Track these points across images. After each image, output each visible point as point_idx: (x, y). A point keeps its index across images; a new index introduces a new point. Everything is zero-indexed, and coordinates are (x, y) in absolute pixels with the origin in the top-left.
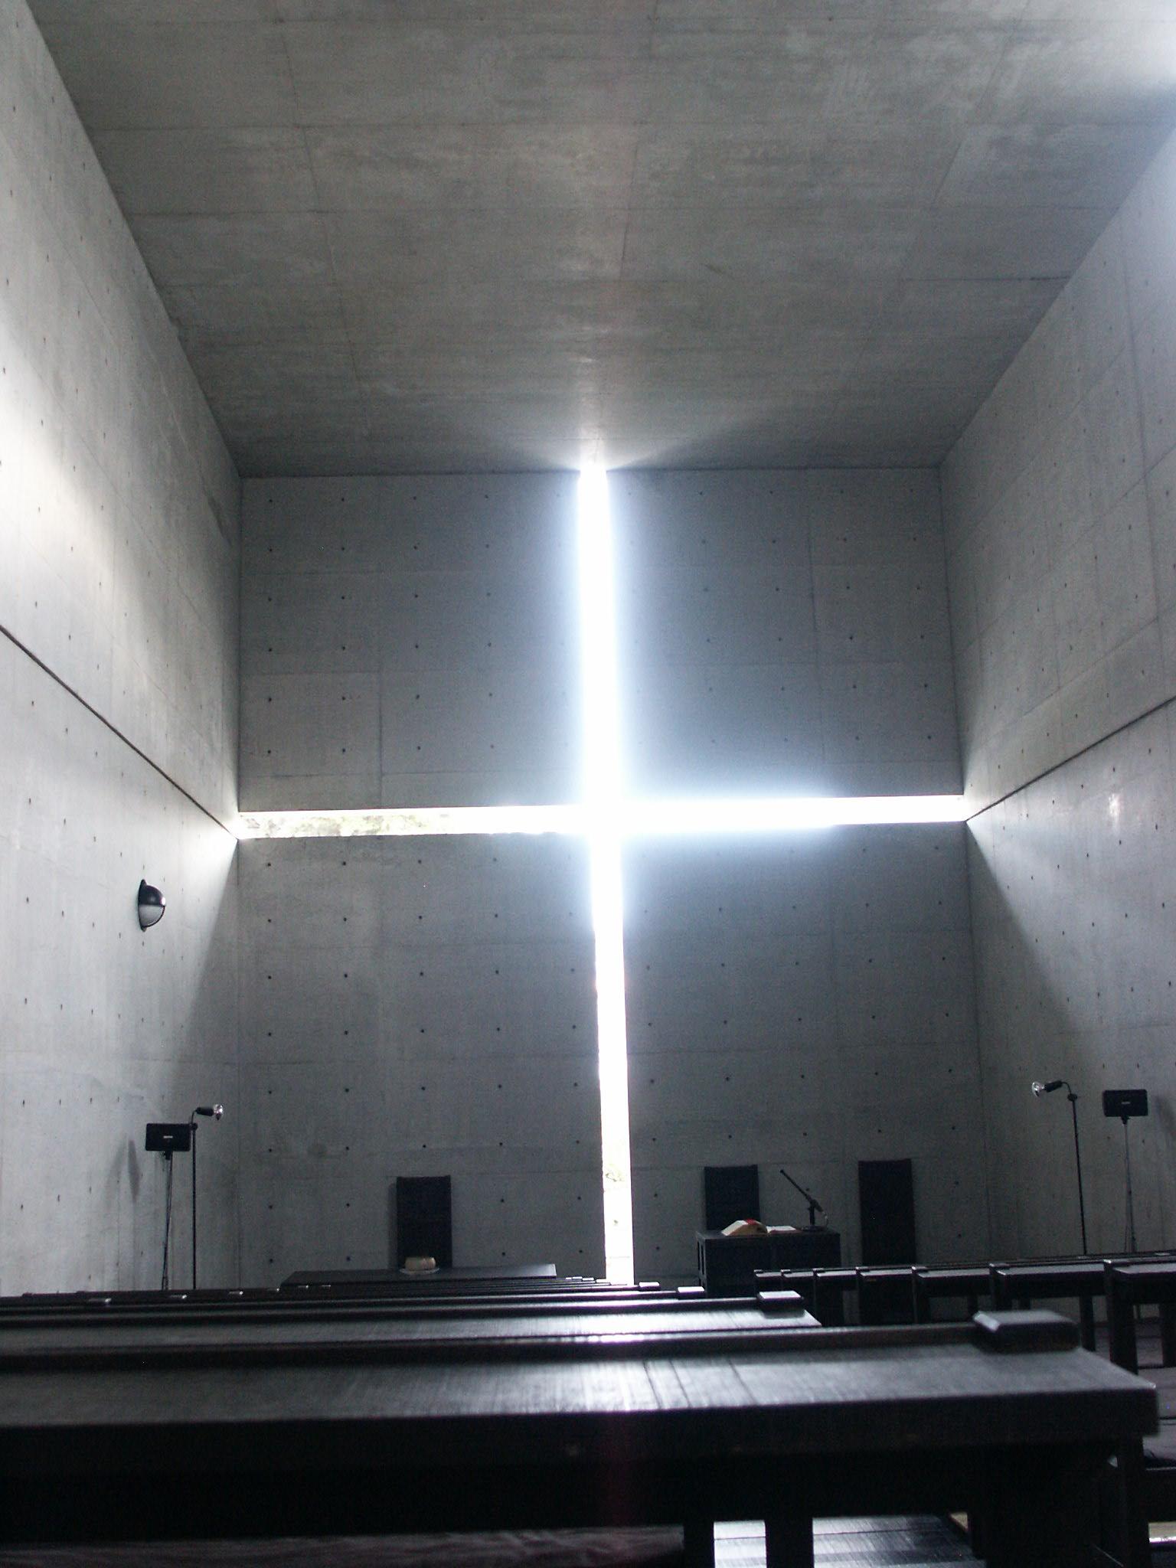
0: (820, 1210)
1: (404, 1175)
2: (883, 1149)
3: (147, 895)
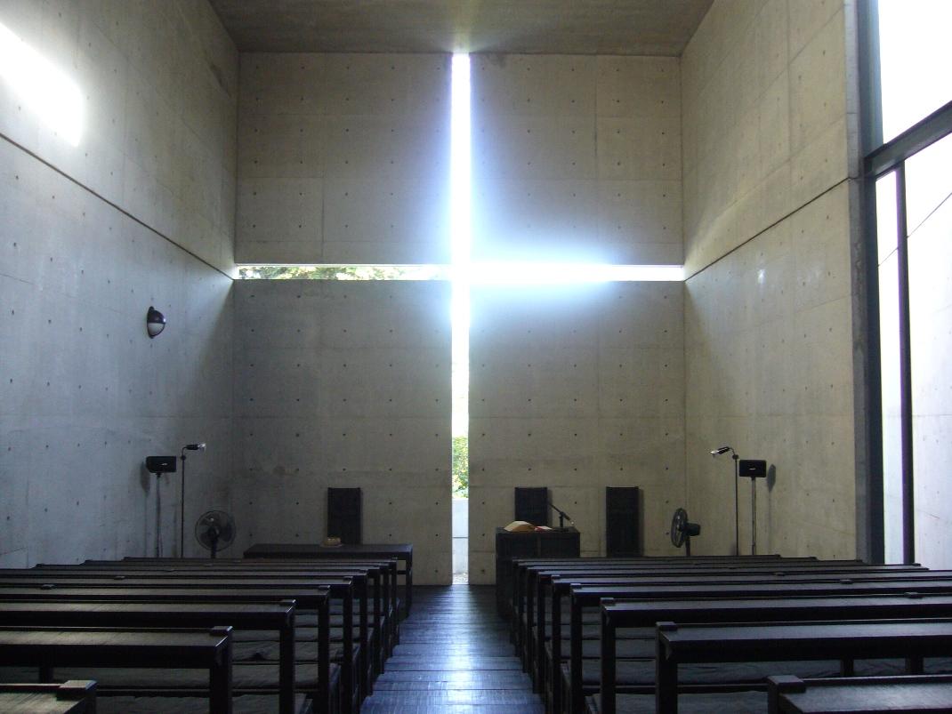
0: (568, 519)
1: (333, 486)
2: (623, 481)
3: (153, 316)
